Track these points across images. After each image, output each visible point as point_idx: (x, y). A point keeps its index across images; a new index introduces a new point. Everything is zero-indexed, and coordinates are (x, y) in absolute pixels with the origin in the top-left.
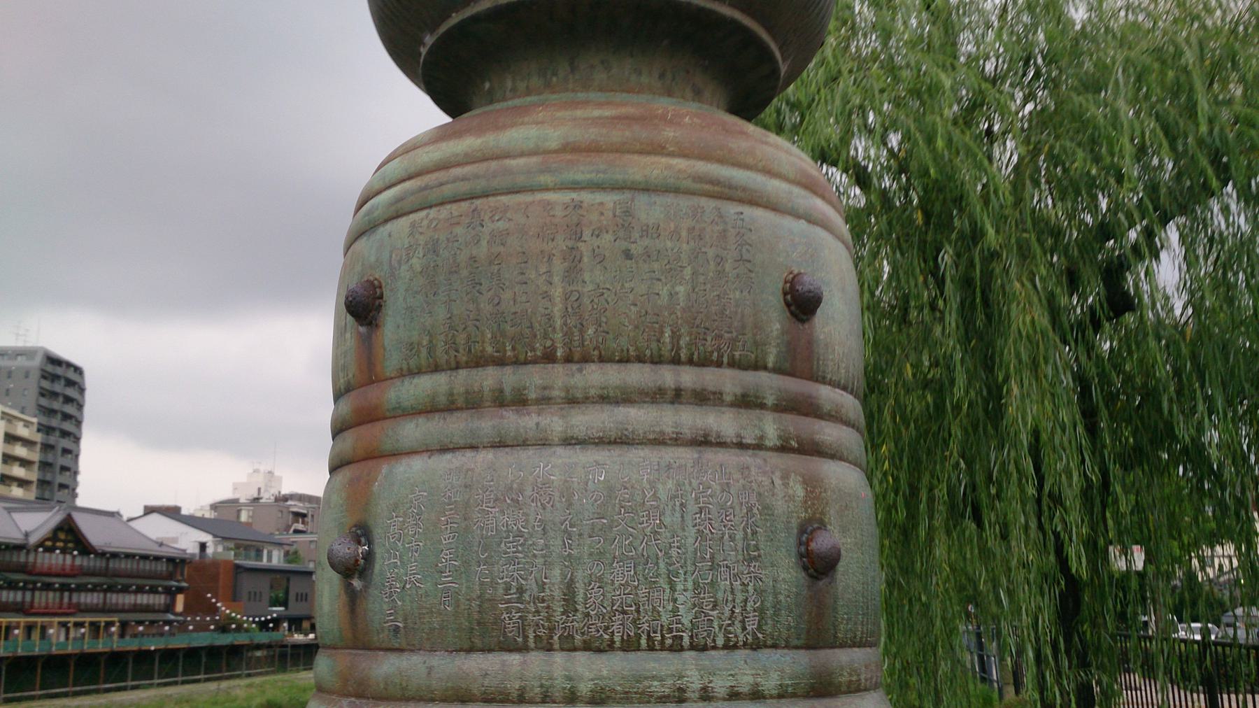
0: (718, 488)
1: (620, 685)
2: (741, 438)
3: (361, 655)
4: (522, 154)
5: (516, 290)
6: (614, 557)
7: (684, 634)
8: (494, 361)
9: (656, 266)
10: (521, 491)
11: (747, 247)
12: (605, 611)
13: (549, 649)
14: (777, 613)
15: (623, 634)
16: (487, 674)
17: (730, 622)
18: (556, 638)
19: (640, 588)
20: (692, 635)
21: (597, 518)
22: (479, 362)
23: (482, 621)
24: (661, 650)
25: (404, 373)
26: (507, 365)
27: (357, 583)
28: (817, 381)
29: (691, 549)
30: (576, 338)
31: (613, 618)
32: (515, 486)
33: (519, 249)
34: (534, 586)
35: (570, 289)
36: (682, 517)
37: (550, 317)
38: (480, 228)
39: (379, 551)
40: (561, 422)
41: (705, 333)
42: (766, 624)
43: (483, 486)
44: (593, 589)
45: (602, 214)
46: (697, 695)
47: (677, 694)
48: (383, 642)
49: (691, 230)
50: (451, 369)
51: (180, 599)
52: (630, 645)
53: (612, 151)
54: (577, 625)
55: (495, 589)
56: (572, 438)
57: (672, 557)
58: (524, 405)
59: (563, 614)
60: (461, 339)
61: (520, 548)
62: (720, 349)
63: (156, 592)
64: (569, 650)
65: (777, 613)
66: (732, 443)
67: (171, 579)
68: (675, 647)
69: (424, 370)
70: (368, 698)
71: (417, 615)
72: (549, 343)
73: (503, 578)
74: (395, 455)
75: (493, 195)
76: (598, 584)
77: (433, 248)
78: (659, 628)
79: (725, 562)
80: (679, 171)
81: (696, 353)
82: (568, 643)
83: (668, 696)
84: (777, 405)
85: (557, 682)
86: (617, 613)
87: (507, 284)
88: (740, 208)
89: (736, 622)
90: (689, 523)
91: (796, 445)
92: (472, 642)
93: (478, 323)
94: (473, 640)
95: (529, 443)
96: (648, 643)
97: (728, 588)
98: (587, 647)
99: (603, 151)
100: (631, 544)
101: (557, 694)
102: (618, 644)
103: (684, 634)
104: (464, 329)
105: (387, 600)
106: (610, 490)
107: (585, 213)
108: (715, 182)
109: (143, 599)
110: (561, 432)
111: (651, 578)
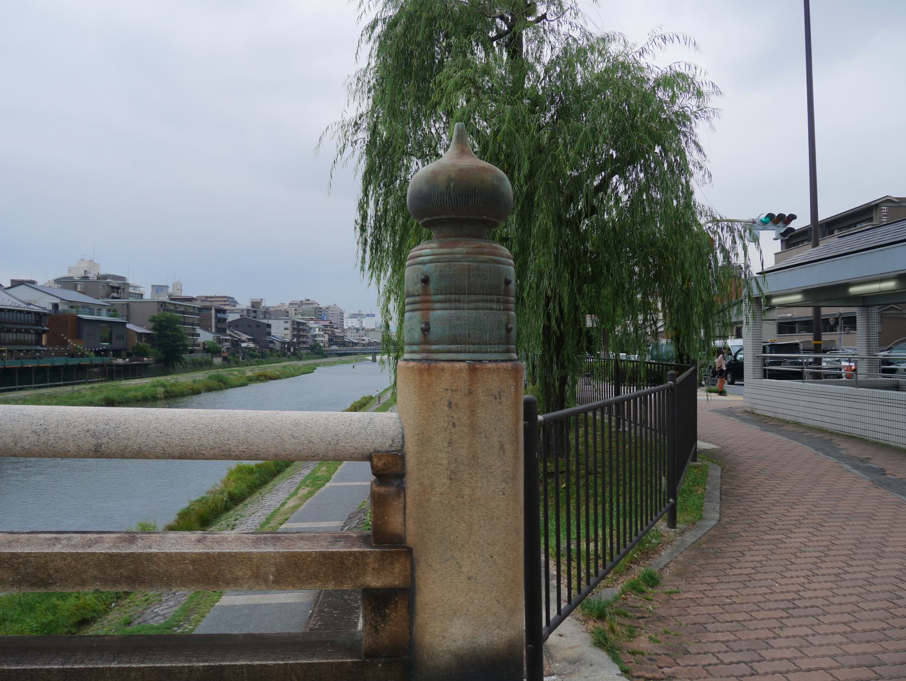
4: (458, 254)
22: (451, 294)
27: (426, 333)
51: (44, 337)
52: (479, 344)
63: (29, 332)
67: (38, 325)
77: (441, 271)
98: (472, 344)
109: (21, 337)
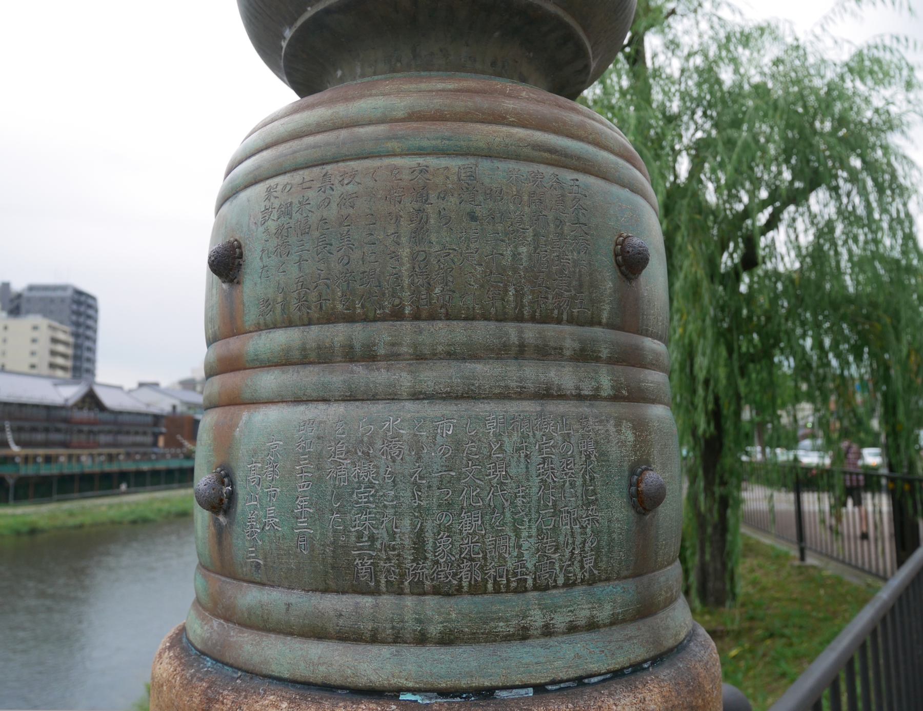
0: (560, 438)
1: (467, 627)
2: (580, 390)
3: (227, 583)
5: (365, 250)
6: (462, 508)
7: (528, 577)
8: (344, 318)
9: (500, 227)
10: (371, 444)
11: (583, 211)
12: (453, 559)
13: (400, 593)
14: (610, 551)
15: (471, 579)
16: (341, 615)
17: (570, 563)
18: (406, 583)
19: (487, 537)
20: (535, 577)
21: (445, 471)
22: (330, 318)
23: (335, 565)
24: (506, 592)
25: (261, 328)
26: (357, 322)
28: (641, 334)
29: (535, 498)
30: (423, 297)
31: (462, 566)
32: (365, 439)
33: (368, 211)
34: (385, 535)
35: (417, 249)
36: (527, 468)
37: (398, 276)
38: (331, 192)
39: (241, 493)
40: (409, 377)
41: (546, 292)
42: (602, 561)
43: (335, 438)
44: (442, 538)
45: (448, 178)
46: (539, 631)
47: (520, 632)
48: (246, 575)
49: (532, 194)
50: (304, 325)
52: (477, 589)
53: (455, 120)
54: (427, 572)
55: (348, 537)
56: (421, 393)
57: (517, 506)
58: (374, 361)
59: (413, 561)
60: (313, 296)
61: (371, 499)
62: (561, 307)
64: (419, 594)
65: (610, 551)
66: (572, 394)
68: (519, 589)
69: (279, 325)
70: (235, 624)
71: (275, 555)
72: (397, 301)
73: (355, 527)
74: (253, 403)
75: (343, 161)
76: (447, 534)
78: (505, 574)
79: (566, 508)
80: (520, 139)
81: (538, 311)
82: (418, 588)
83: (513, 634)
84: (610, 357)
85: (407, 624)
86: (465, 561)
87: (356, 244)
88: (575, 175)
89: (576, 563)
90: (533, 472)
91: (626, 394)
92: (328, 584)
93: (328, 281)
94: (327, 582)
95: (378, 397)
96: (494, 588)
97: (569, 532)
98: (436, 591)
99: (447, 120)
100: (478, 495)
101: (408, 636)
102: (466, 589)
103: (528, 577)
104: (316, 287)
105: (249, 538)
106: (458, 444)
107: (431, 177)
108: (552, 150)
109: (139, 439)
110: (410, 387)
111: (498, 526)
